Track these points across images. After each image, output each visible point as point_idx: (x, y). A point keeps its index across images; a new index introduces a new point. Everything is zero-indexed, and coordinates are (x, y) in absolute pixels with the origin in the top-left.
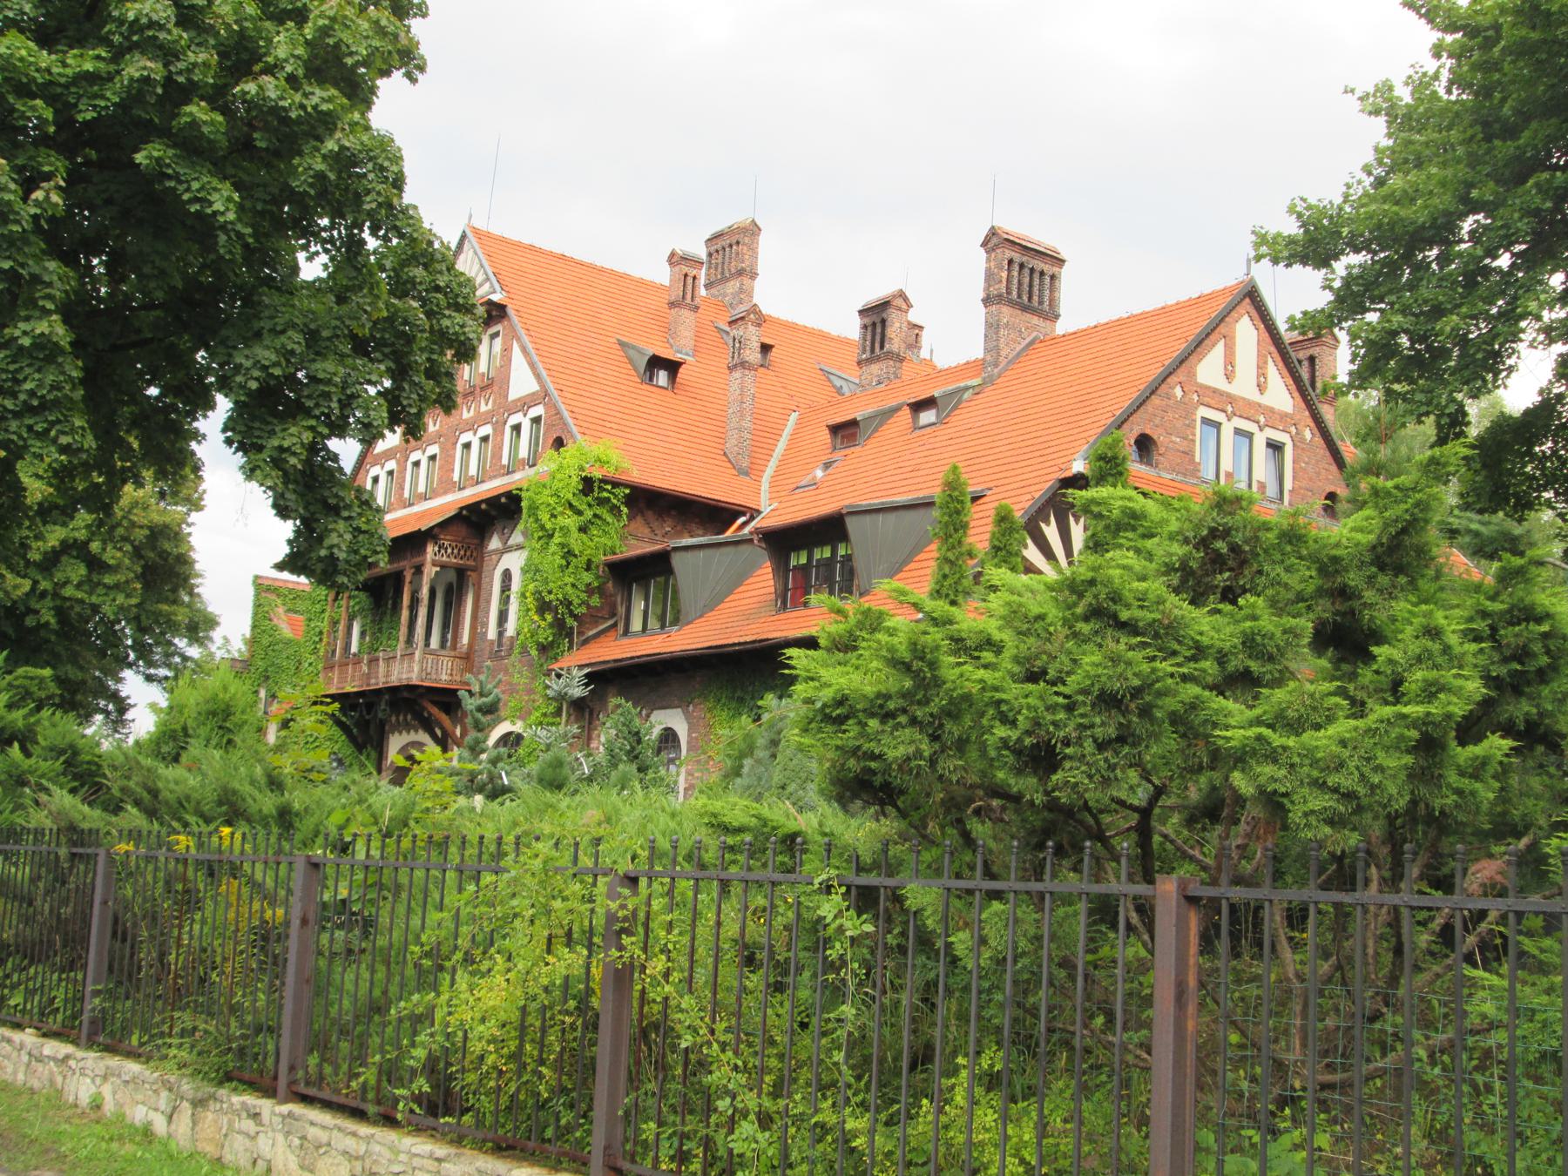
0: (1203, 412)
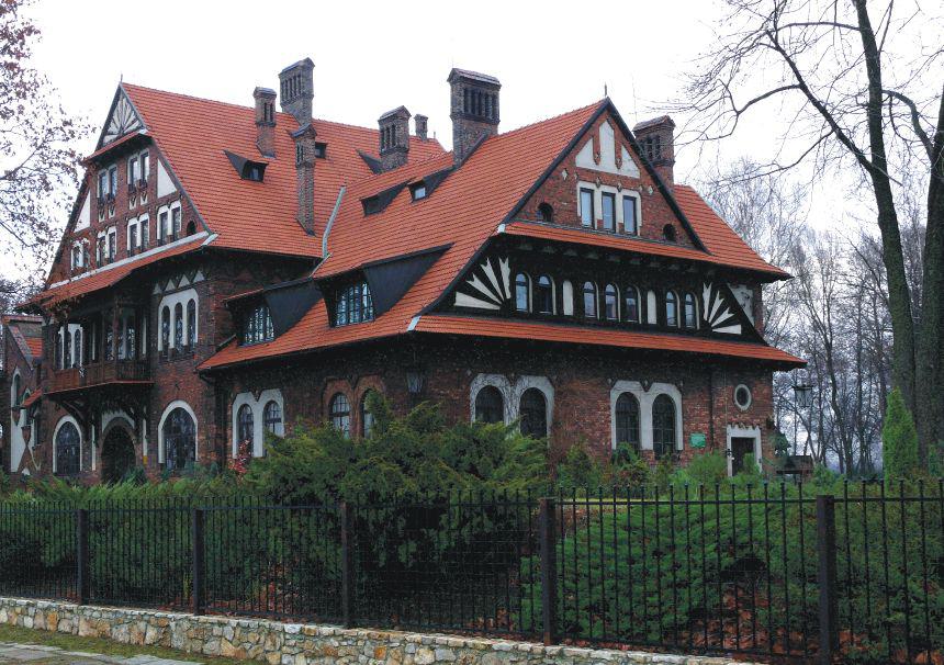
0: (581, 184)
